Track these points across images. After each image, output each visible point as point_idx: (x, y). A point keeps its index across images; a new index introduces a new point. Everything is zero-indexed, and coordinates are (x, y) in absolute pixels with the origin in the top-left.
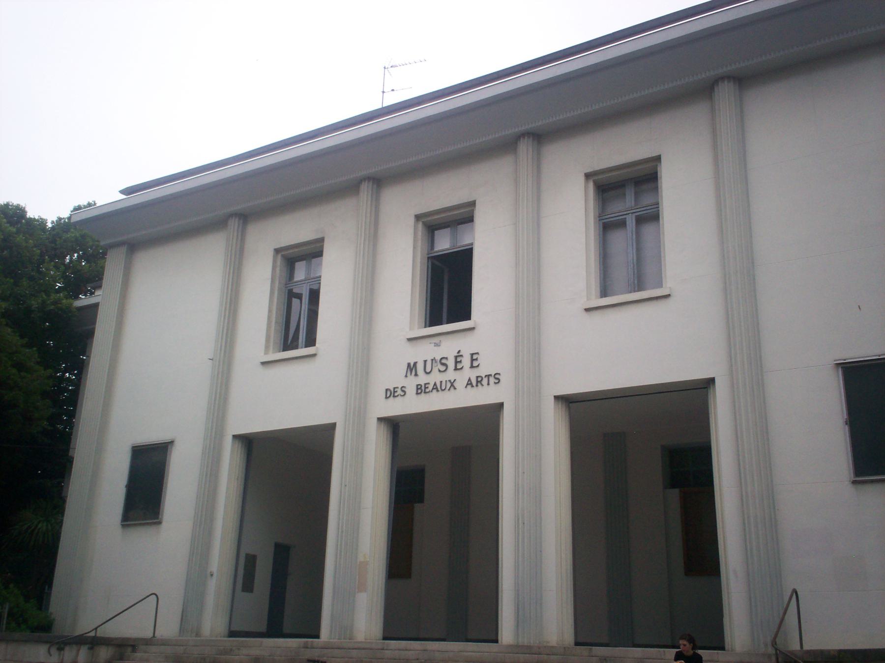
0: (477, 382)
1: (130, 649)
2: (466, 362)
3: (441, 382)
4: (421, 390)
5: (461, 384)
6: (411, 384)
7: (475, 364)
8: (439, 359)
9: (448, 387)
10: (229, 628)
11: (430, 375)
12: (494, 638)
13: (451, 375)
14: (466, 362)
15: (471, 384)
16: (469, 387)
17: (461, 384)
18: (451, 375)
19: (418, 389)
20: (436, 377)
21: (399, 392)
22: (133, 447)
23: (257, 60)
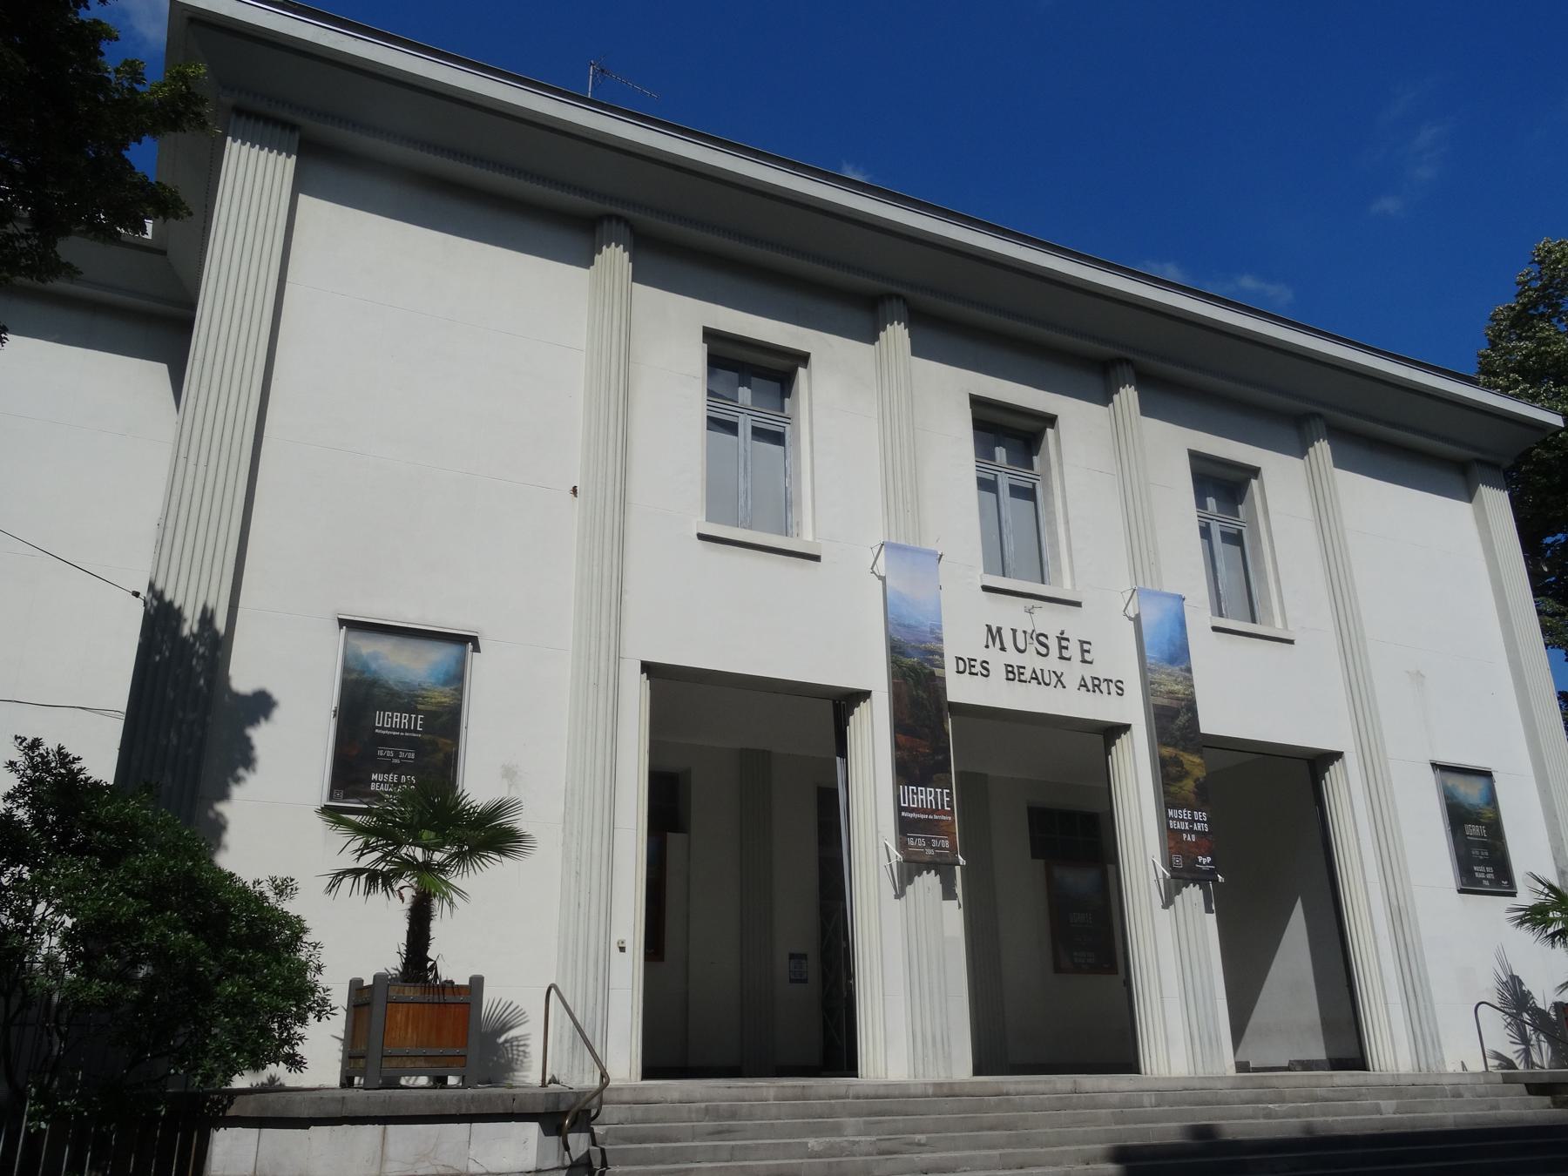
0: (1094, 685)
1: (470, 646)
2: (1074, 651)
3: (517, 1007)
4: (1013, 673)
5: (1072, 680)
6: (997, 659)
7: (1088, 657)
8: (1038, 632)
9: (1053, 683)
10: (1557, 867)
11: (1026, 653)
12: (1355, 1054)
13: (1052, 663)
14: (1074, 651)
15: (1085, 686)
16: (1083, 689)
17: (1072, 680)
18: (1052, 663)
19: (1008, 672)
20: (1031, 661)
21: (978, 669)
22: (546, 1135)
23: (574, 490)
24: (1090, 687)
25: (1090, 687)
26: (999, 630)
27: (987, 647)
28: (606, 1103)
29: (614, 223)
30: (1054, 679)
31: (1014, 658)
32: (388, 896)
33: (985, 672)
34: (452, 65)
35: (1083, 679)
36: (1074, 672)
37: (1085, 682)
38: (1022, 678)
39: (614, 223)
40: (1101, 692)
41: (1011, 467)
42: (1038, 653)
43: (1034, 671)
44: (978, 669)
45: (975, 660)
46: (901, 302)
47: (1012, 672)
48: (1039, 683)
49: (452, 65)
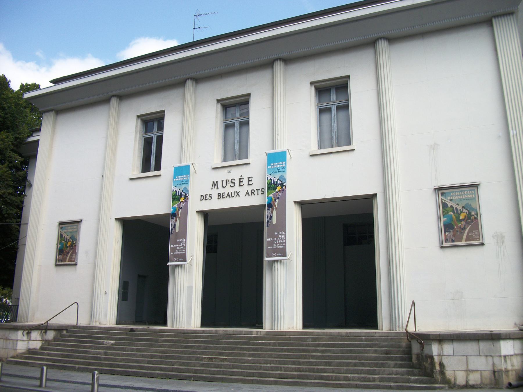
2: (245, 181)
4: (220, 196)
5: (243, 193)
6: (215, 192)
7: (250, 183)
13: (237, 188)
14: (245, 181)
16: (247, 195)
17: (243, 193)
18: (237, 188)
19: (218, 196)
20: (228, 190)
24: (250, 194)
25: (250, 194)
26: (217, 182)
27: (212, 189)
28: (3, 347)
29: (382, 40)
30: (236, 194)
31: (221, 190)
32: (489, 331)
33: (210, 198)
34: (177, 53)
35: (247, 191)
36: (243, 191)
37: (248, 192)
38: (224, 197)
39: (382, 40)
40: (254, 195)
41: (146, 134)
42: (231, 186)
43: (228, 193)
44: (208, 197)
45: (207, 195)
46: (385, 39)
47: (220, 196)
48: (230, 197)
49: (177, 53)
